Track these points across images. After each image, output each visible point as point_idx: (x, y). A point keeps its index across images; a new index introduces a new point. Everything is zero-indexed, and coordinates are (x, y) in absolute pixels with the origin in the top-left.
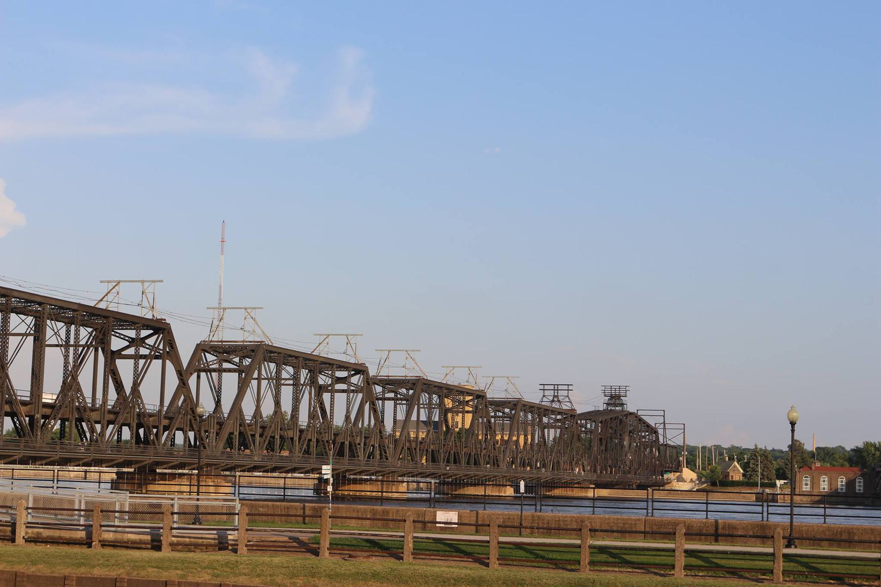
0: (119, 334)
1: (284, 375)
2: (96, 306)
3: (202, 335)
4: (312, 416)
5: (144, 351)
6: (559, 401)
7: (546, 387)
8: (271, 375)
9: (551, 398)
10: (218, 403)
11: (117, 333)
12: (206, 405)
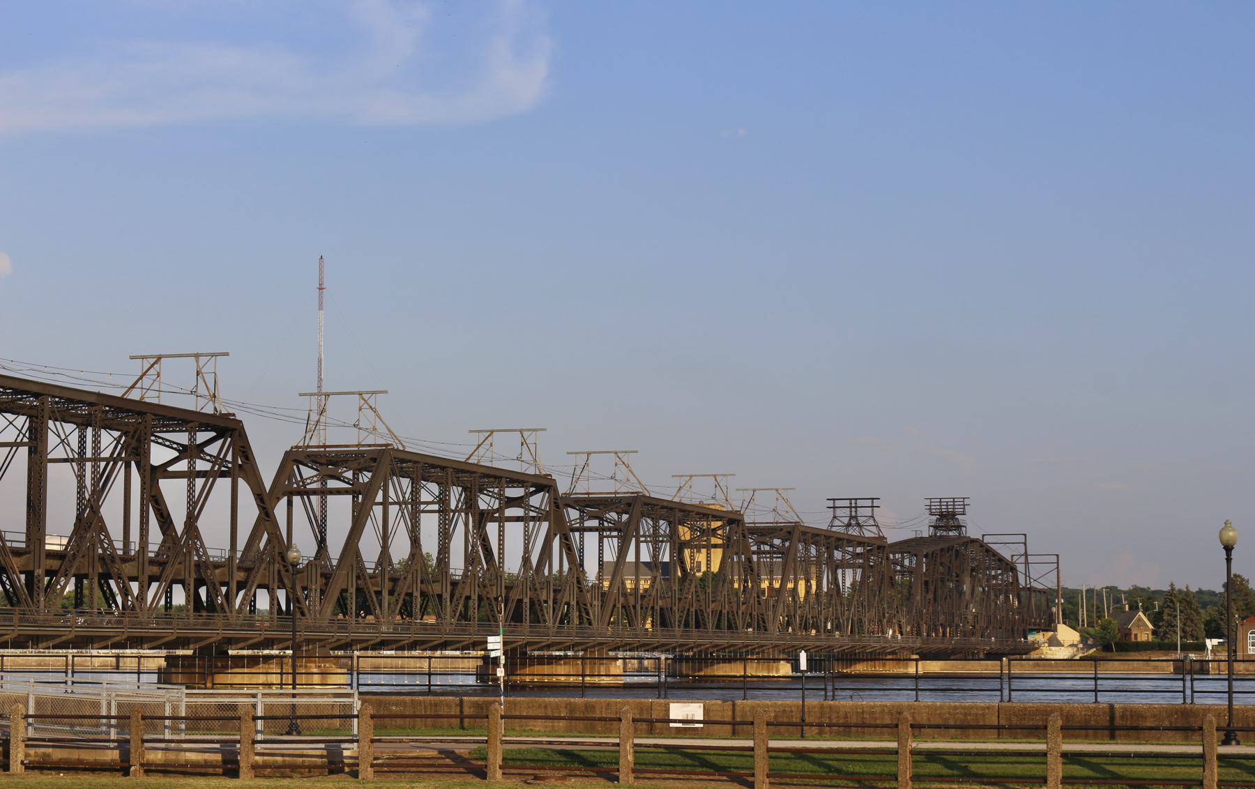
0: (163, 439)
1: (425, 496)
2: (125, 397)
3: (293, 437)
4: (470, 559)
5: (202, 465)
6: (858, 525)
8: (404, 497)
9: (846, 520)
10: (322, 543)
11: (160, 438)
12: (303, 546)
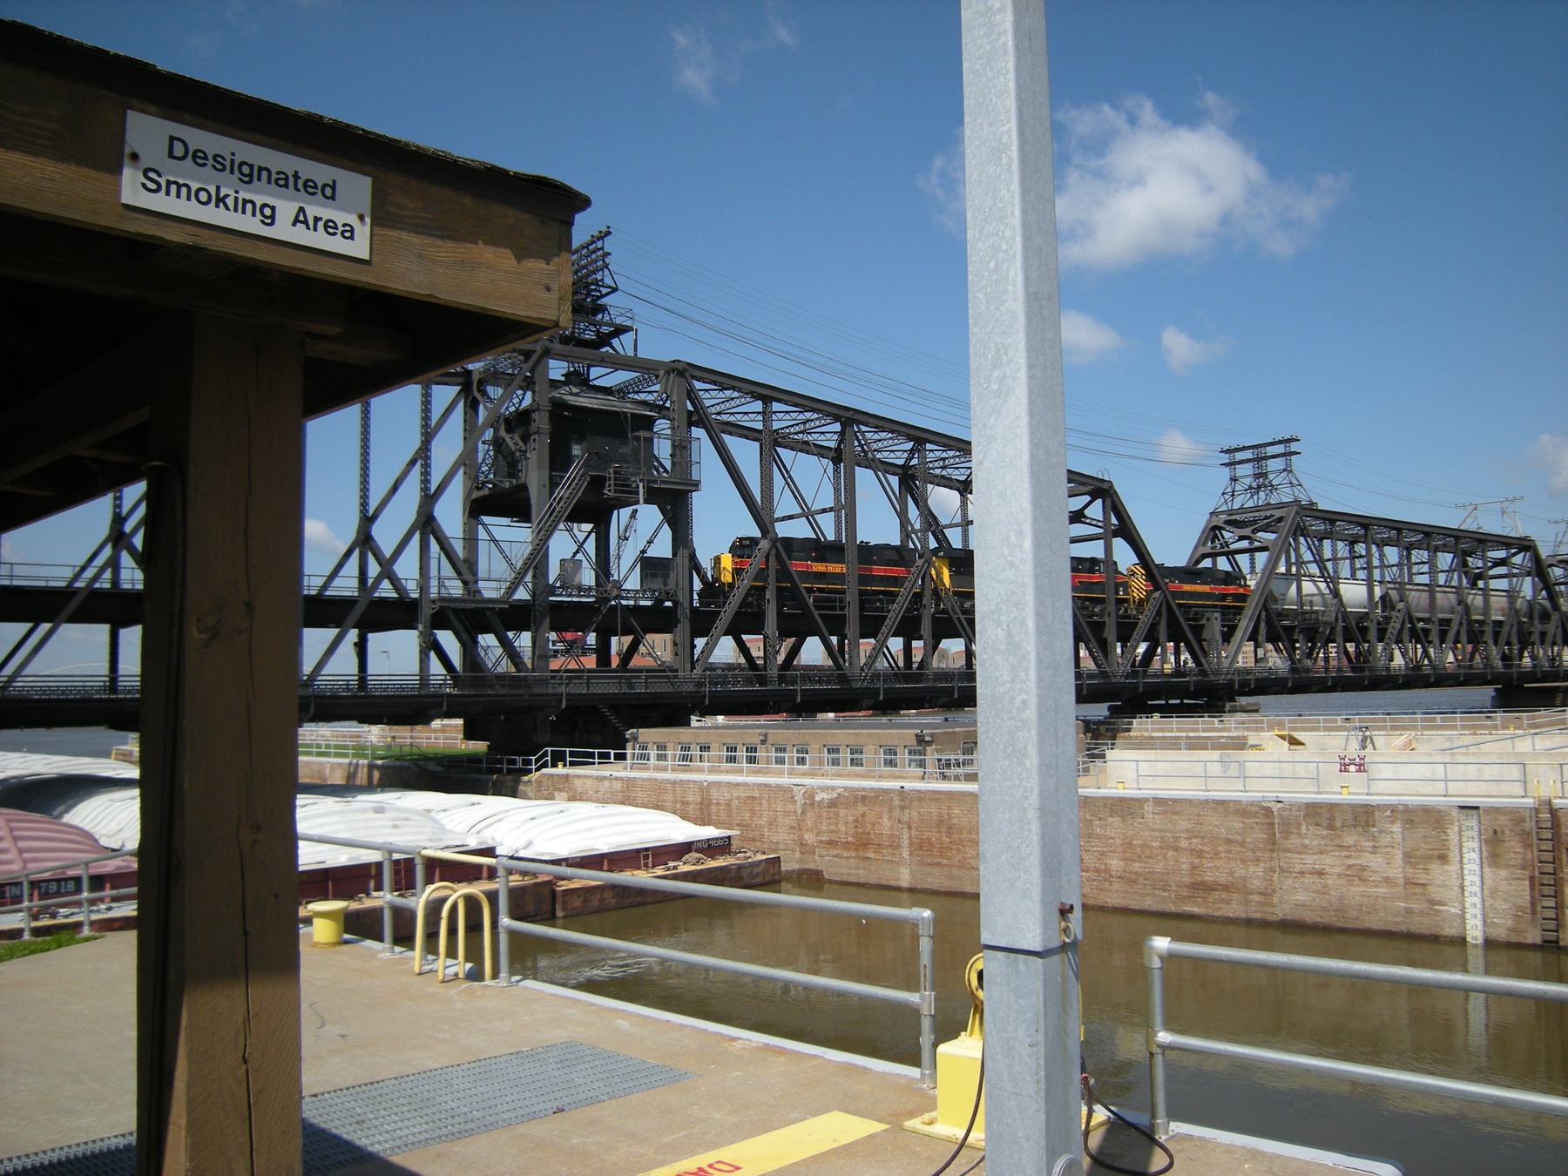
7: (1239, 456)
